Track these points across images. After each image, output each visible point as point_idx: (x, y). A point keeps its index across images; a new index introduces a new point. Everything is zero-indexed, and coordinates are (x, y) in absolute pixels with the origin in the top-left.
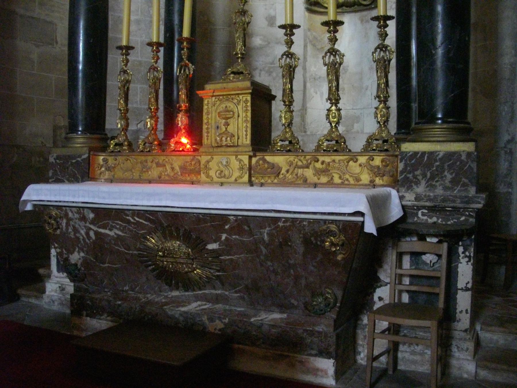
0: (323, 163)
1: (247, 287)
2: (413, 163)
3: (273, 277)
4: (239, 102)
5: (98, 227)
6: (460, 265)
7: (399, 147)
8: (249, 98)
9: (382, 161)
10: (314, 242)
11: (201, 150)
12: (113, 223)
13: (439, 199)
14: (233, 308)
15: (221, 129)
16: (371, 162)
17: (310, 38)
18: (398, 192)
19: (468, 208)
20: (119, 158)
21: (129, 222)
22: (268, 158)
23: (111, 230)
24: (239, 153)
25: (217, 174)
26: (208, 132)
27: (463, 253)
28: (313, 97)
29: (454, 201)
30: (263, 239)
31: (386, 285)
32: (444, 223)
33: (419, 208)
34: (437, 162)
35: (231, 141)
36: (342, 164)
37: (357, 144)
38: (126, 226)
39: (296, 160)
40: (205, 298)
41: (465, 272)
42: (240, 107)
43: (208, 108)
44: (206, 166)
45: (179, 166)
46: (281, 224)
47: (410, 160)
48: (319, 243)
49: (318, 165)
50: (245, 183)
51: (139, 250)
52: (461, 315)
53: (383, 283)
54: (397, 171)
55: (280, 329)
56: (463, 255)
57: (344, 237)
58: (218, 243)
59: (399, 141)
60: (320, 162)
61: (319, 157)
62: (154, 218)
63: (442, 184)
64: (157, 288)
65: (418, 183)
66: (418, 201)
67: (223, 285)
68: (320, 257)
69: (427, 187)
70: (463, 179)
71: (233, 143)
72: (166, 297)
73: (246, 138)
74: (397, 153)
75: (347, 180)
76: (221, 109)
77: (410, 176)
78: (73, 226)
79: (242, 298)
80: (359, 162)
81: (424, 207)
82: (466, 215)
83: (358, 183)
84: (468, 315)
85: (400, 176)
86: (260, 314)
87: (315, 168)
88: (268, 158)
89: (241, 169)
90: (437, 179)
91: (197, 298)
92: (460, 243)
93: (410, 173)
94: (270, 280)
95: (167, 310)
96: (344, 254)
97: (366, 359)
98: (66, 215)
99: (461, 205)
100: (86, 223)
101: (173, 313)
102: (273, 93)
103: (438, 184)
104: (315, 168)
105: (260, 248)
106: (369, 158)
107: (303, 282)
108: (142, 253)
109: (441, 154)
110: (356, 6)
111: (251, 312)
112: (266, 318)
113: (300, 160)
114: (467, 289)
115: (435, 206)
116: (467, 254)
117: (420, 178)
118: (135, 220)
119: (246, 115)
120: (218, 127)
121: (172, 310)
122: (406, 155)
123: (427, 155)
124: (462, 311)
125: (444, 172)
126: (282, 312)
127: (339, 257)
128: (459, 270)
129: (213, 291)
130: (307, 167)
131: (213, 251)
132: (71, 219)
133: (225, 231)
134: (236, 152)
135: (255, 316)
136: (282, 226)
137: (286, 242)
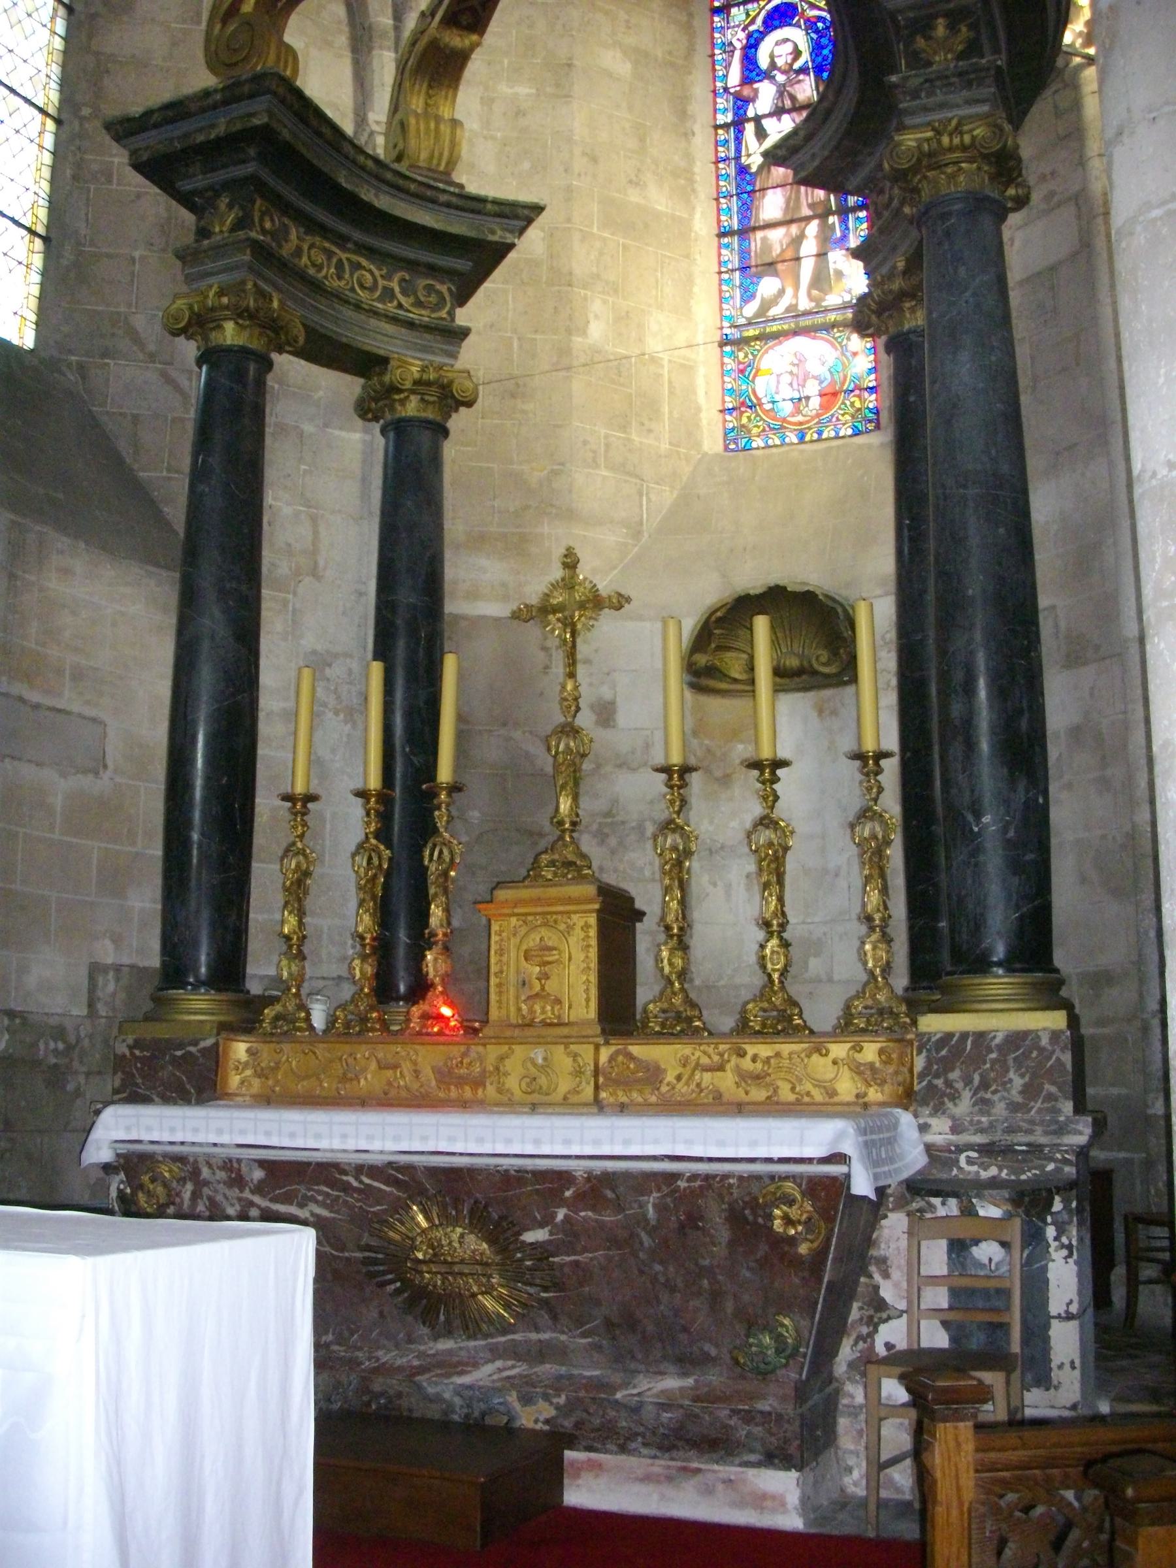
0: (754, 1059)
1: (609, 1324)
2: (943, 1057)
3: (665, 1297)
4: (570, 928)
5: (271, 1200)
6: (1051, 1265)
7: (914, 1023)
8: (592, 920)
9: (881, 1052)
10: (751, 1218)
11: (488, 1031)
12: (309, 1190)
13: (1000, 1127)
14: (576, 1372)
15: (531, 988)
16: (857, 1055)
17: (699, 753)
18: (916, 1116)
19: (1060, 1145)
20: (286, 1047)
21: (346, 1188)
22: (635, 1050)
23: (301, 1206)
24: (572, 1040)
25: (524, 1085)
26: (500, 993)
27: (1056, 1239)
28: (707, 895)
29: (1029, 1132)
30: (645, 1215)
31: (900, 1316)
32: (1013, 1177)
33: (960, 1149)
34: (992, 1052)
35: (553, 1013)
36: (796, 1060)
37: (822, 1012)
38: (338, 1197)
39: (698, 1054)
40: (514, 1352)
41: (1064, 1279)
42: (572, 940)
43: (502, 940)
44: (497, 1069)
45: (433, 1068)
46: (682, 1184)
47: (938, 1051)
48: (760, 1220)
49: (747, 1064)
50: (586, 1105)
51: (368, 1248)
52: (1060, 1373)
53: (892, 1313)
54: (911, 1071)
55: (681, 1411)
56: (1057, 1243)
57: (812, 1206)
58: (546, 1229)
59: (916, 1007)
60: (748, 1057)
61: (747, 1047)
62: (406, 1178)
63: (1004, 1098)
64: (401, 1335)
65: (955, 1097)
66: (958, 1134)
67: (555, 1318)
68: (763, 1248)
69: (974, 1105)
70: (1047, 1086)
71: (559, 1017)
72: (421, 1355)
73: (587, 1006)
74: (910, 1036)
75: (808, 1094)
76: (531, 944)
77: (939, 1082)
78: (210, 1199)
79: (598, 1347)
80: (832, 1056)
81: (970, 1147)
82: (1055, 1160)
83: (832, 1100)
84: (1077, 1373)
85: (919, 1083)
86: (636, 1381)
87: (739, 1071)
88: (635, 1050)
89: (578, 1073)
90: (993, 1088)
91: (496, 1353)
92: (1049, 1219)
93: (937, 1076)
94: (659, 1302)
95: (425, 1384)
96: (812, 1242)
97: (864, 1482)
98: (195, 1173)
99: (1043, 1140)
100: (241, 1192)
101: (438, 1389)
102: (639, 904)
103: (996, 1098)
104: (739, 1071)
105: (638, 1235)
106: (853, 1048)
107: (729, 1306)
108: (373, 1255)
109: (1000, 1038)
110: (804, 677)
111: (617, 1378)
112: (649, 1389)
113: (705, 1053)
114: (1069, 1317)
115: (992, 1144)
116: (1064, 1240)
117: (959, 1085)
118: (361, 1182)
119: (587, 957)
120: (524, 984)
121: (436, 1384)
122: (929, 1040)
123: (970, 1039)
124: (1062, 1364)
125: (1007, 1071)
126: (685, 1375)
127: (803, 1249)
128: (1051, 1275)
129: (534, 1336)
130: (721, 1068)
131: (534, 1245)
132: (206, 1183)
133: (563, 1202)
134: (566, 1037)
135: (626, 1385)
136: (685, 1189)
137: (693, 1220)
